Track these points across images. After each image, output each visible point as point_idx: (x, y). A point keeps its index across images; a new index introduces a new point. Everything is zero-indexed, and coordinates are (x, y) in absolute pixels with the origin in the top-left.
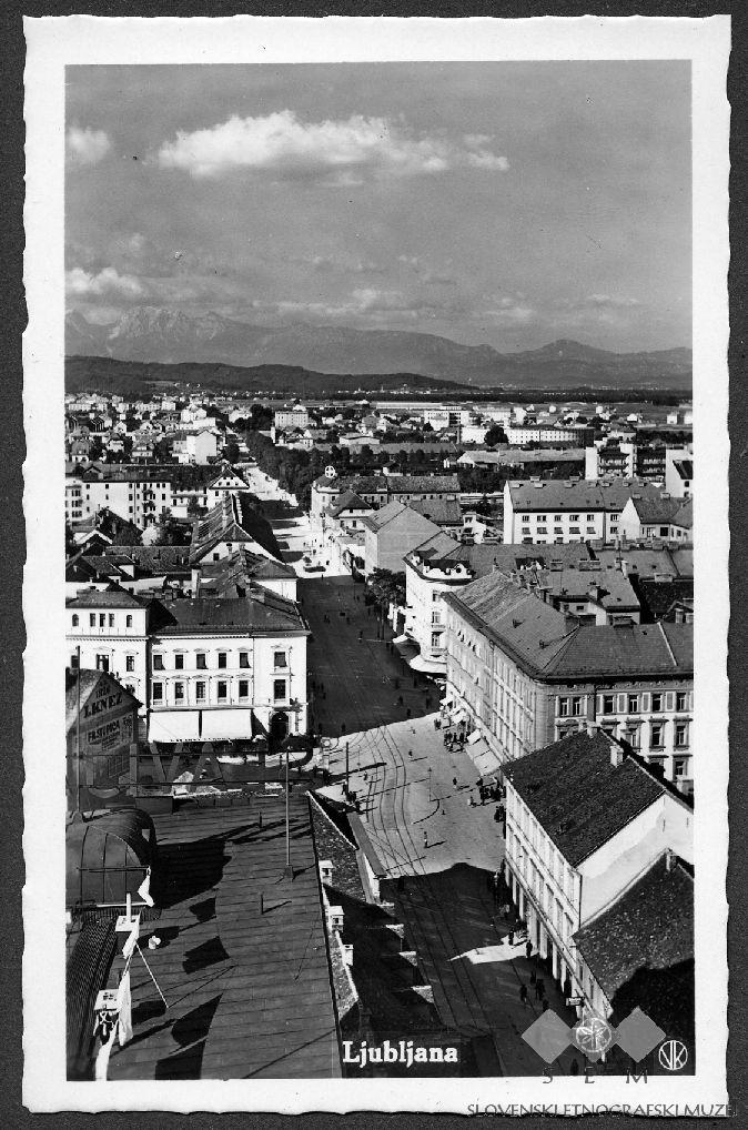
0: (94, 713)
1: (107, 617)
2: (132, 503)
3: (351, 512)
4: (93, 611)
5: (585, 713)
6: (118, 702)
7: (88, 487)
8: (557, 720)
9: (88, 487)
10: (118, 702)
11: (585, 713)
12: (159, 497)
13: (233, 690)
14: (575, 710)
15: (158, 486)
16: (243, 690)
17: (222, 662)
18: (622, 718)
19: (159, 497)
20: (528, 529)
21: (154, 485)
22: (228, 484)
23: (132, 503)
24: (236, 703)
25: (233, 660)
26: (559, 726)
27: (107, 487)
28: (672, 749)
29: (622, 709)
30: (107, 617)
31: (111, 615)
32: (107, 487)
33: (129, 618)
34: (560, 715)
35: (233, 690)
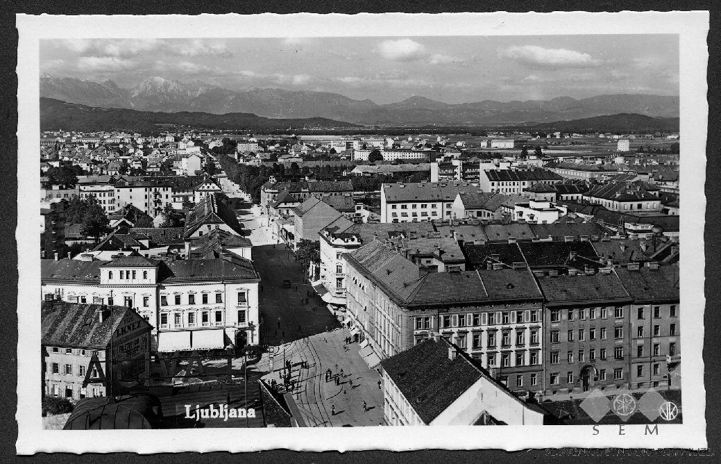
4: (122, 269)
9: (118, 191)
25: (212, 298)
26: (417, 335)
27: (131, 191)
32: (131, 191)
34: (417, 329)
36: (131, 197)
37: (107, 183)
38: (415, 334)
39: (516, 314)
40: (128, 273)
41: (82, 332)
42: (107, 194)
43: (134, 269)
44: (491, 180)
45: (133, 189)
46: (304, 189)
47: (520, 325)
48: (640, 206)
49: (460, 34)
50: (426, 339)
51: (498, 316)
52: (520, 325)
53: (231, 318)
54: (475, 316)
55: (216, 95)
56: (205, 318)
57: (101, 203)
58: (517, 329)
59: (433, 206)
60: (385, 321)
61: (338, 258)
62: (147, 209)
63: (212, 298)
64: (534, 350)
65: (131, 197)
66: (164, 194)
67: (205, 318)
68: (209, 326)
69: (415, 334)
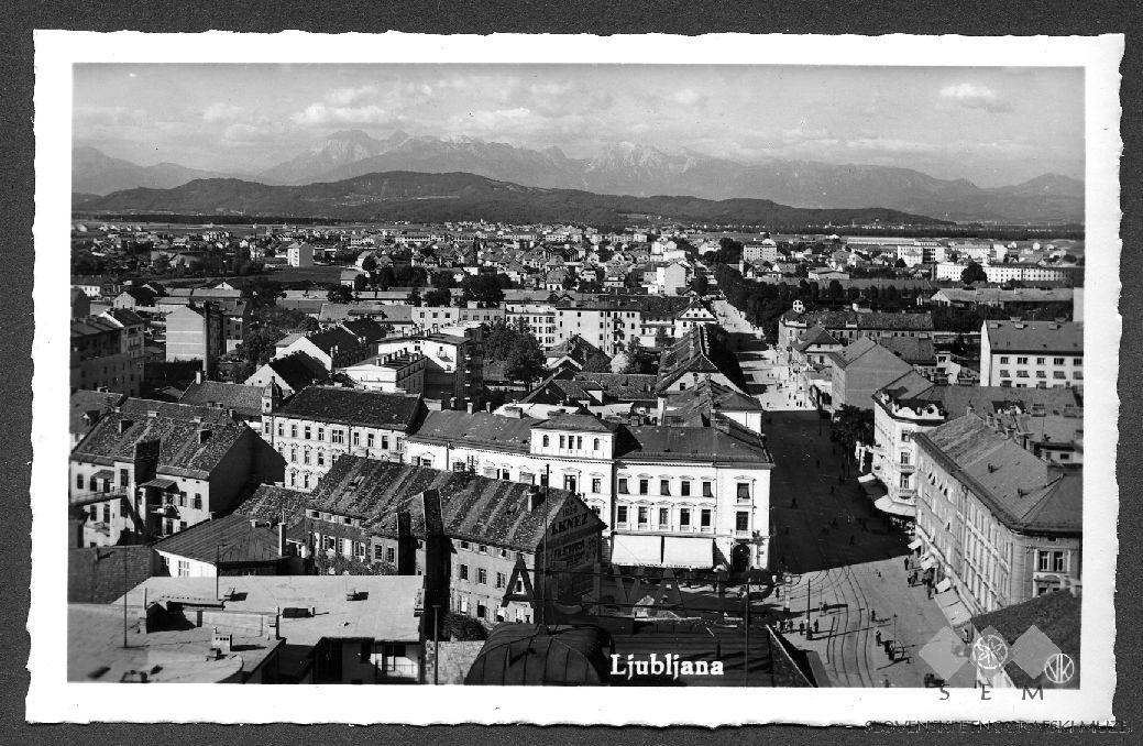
2: (602, 331)
3: (819, 346)
7: (561, 314)
8: (1036, 575)
9: (561, 314)
13: (695, 518)
14: (1058, 566)
15: (628, 315)
16: (706, 520)
23: (602, 331)
25: (696, 488)
26: (1039, 581)
27: (579, 315)
32: (579, 315)
33: (596, 441)
35: (695, 518)
38: (1035, 577)
45: (583, 313)
46: (849, 323)
50: (1055, 589)
60: (982, 550)
61: (903, 439)
63: (696, 488)
69: (1035, 577)
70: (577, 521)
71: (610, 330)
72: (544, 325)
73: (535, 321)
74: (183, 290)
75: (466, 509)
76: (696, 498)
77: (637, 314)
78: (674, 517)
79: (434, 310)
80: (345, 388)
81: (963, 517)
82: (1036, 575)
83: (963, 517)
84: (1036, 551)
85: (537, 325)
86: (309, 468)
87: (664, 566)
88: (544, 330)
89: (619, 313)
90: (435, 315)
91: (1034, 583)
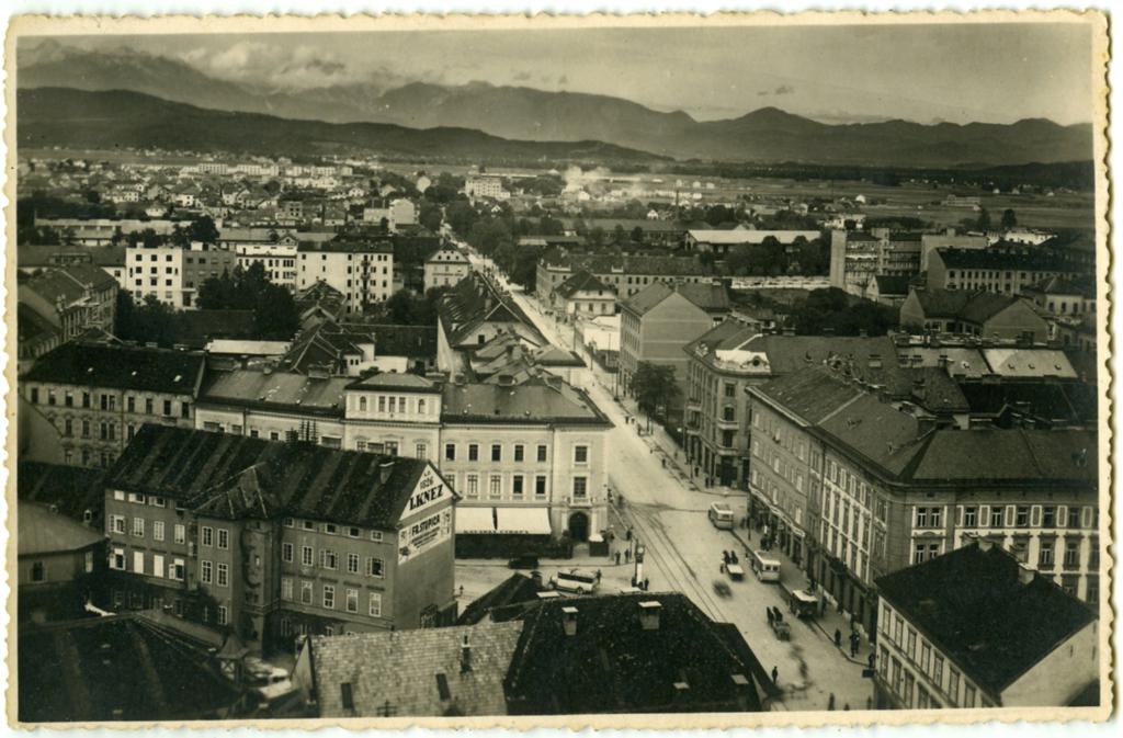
0: (418, 505)
1: (387, 401)
2: (350, 277)
3: (601, 294)
4: (382, 394)
5: (945, 525)
6: (440, 495)
7: (304, 257)
8: (913, 532)
9: (304, 257)
10: (440, 495)
11: (945, 525)
12: (380, 271)
13: (529, 486)
14: (936, 523)
15: (380, 258)
16: (540, 488)
17: (496, 455)
18: (1009, 532)
19: (380, 271)
20: (170, 292)
21: (376, 256)
22: (448, 258)
23: (350, 277)
24: (534, 500)
25: (531, 453)
26: (917, 538)
27: (324, 257)
28: (1062, 568)
29: (1010, 523)
30: (387, 401)
31: (401, 399)
32: (324, 257)
33: (363, 400)
34: (918, 527)
35: (529, 486)
36: (324, 269)
37: (262, 242)
38: (913, 534)
39: (989, 511)
40: (392, 400)
41: (354, 503)
42: (281, 261)
43: (402, 395)
44: (948, 266)
45: (329, 255)
46: (615, 267)
47: (1073, 532)
48: (696, 281)
49: (996, 21)
51: (1037, 510)
52: (1073, 532)
53: (560, 488)
54: (1046, 509)
55: (417, 92)
56: (518, 487)
57: (271, 276)
58: (1042, 537)
59: (374, 270)
62: (349, 290)
63: (531, 453)
64: (1070, 576)
65: (324, 269)
66: (375, 263)
67: (518, 487)
68: (525, 500)
69: (913, 534)
70: (433, 493)
71: (357, 276)
72: (281, 269)
73: (271, 264)
74: (524, 310)
75: (306, 483)
76: (530, 467)
77: (390, 257)
78: (507, 486)
79: (153, 251)
80: (163, 350)
81: (819, 476)
82: (913, 532)
83: (819, 476)
84: (914, 508)
85: (275, 269)
86: (90, 442)
87: (498, 532)
88: (281, 275)
89: (369, 256)
90: (154, 258)
91: (912, 541)
